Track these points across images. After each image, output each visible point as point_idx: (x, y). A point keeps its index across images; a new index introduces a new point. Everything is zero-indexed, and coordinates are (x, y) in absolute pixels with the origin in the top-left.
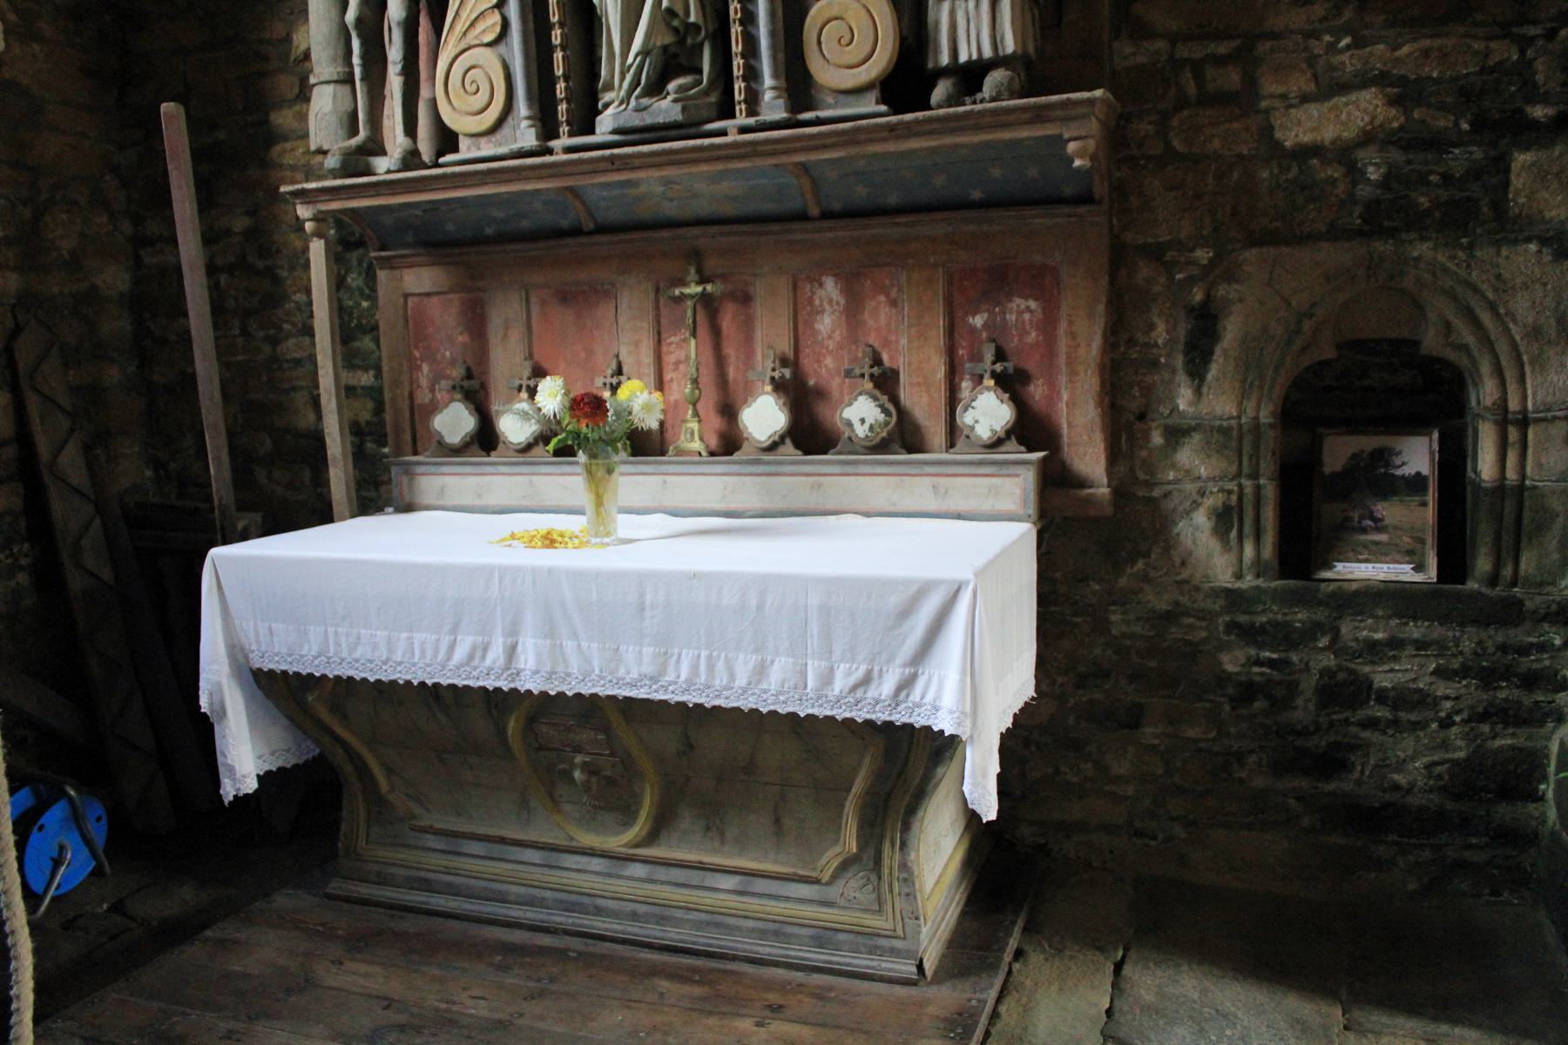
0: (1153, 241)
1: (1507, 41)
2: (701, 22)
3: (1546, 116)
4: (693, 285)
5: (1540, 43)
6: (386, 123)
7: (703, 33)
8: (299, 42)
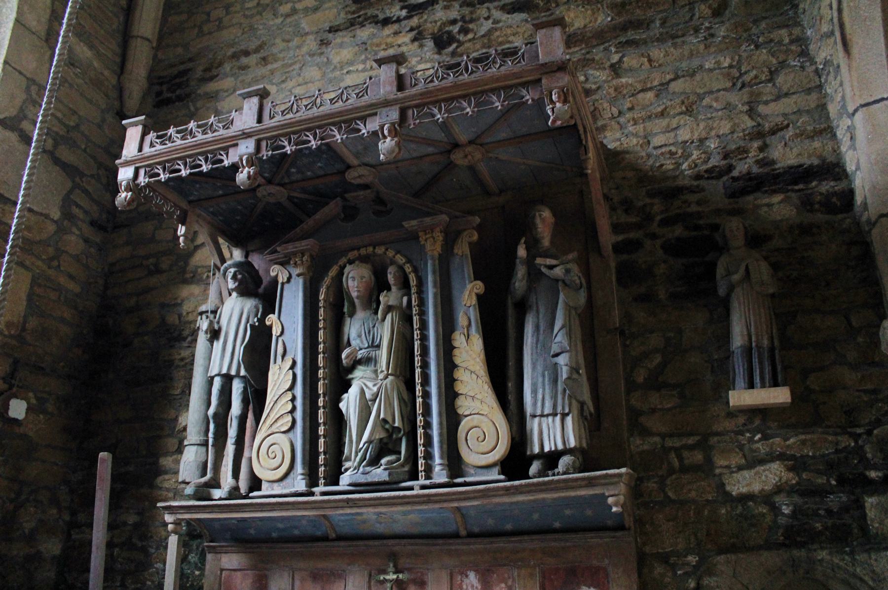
0: (662, 551)
1: (846, 436)
2: (401, 427)
3: (877, 477)
4: (391, 573)
5: (865, 437)
6: (223, 469)
7: (402, 432)
8: (182, 421)
